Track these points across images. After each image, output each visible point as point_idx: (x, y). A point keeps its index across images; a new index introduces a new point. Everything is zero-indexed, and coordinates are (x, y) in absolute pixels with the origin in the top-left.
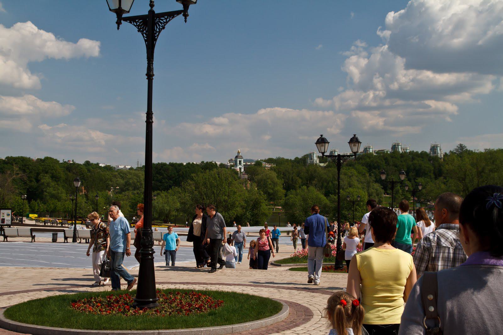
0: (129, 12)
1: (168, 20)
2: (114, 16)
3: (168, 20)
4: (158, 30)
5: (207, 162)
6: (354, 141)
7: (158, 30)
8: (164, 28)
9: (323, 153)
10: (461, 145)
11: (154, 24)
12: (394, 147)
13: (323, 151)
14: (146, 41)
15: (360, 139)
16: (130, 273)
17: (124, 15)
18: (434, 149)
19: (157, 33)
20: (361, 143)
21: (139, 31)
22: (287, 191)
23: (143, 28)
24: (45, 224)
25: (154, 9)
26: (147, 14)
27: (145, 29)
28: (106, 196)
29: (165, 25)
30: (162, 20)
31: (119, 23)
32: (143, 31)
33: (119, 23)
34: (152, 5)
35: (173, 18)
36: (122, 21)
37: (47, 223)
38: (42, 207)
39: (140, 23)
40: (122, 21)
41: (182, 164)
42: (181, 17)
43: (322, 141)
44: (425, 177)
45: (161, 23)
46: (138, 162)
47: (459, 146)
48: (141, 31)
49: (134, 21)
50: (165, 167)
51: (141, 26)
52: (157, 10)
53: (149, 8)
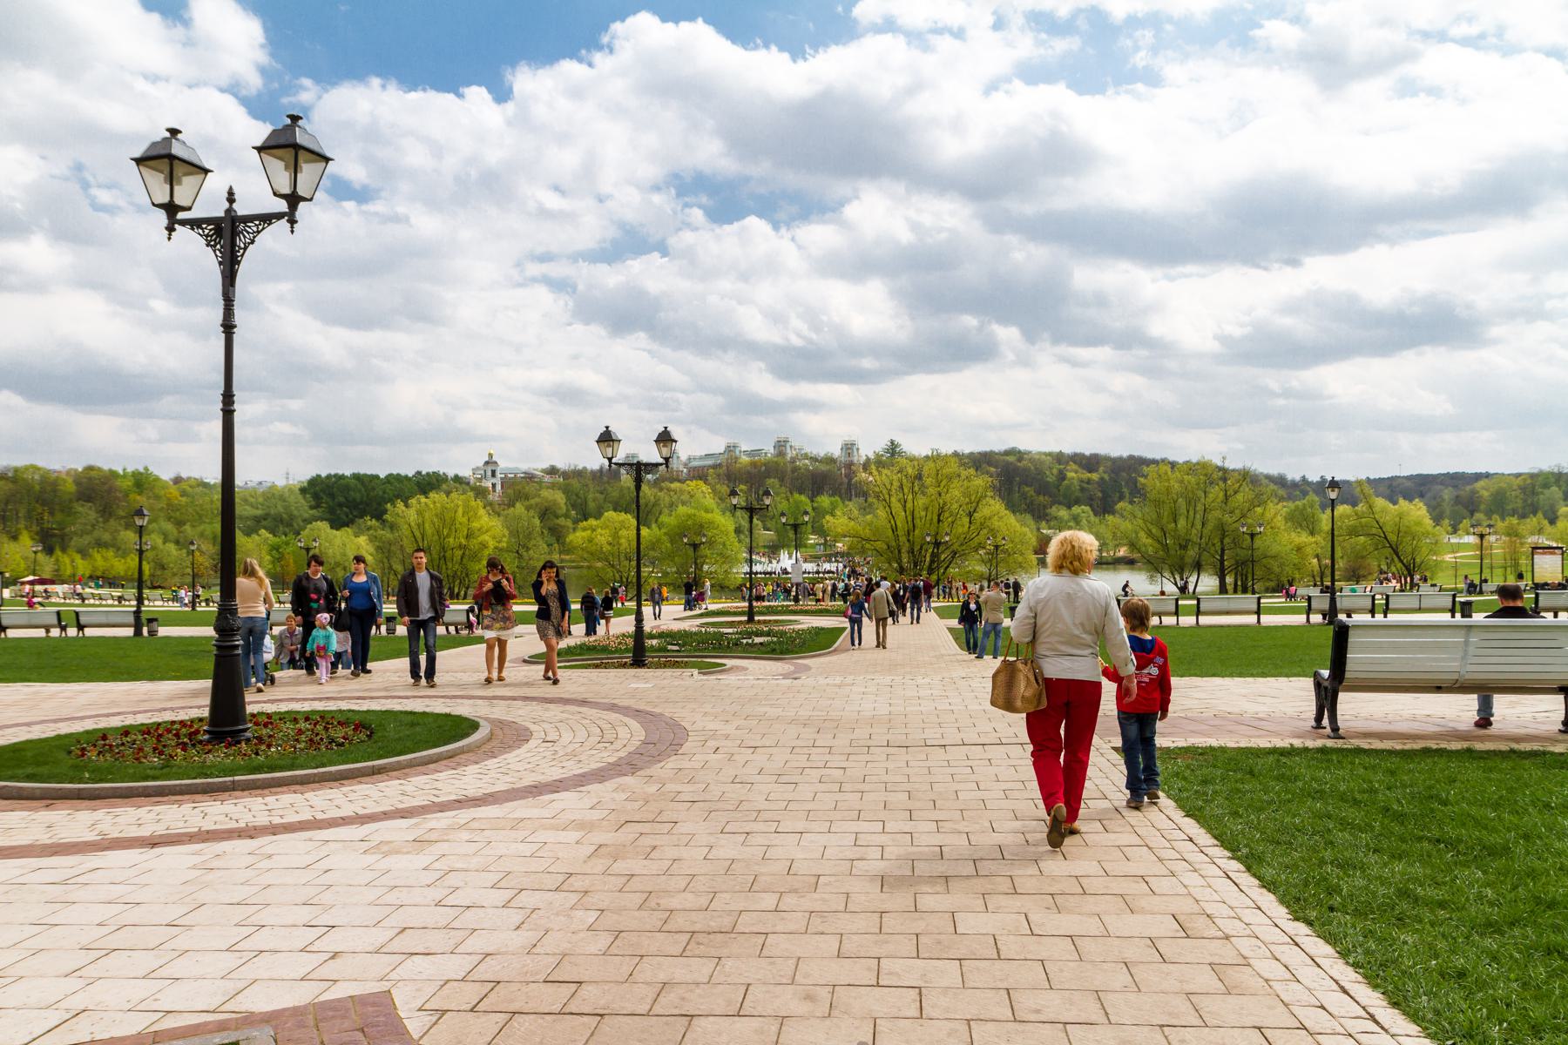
0: (189, 209)
1: (261, 227)
2: (161, 217)
3: (261, 227)
4: (242, 245)
5: (428, 474)
6: (665, 438)
7: (242, 245)
8: (253, 242)
9: (610, 460)
10: (892, 442)
11: (234, 233)
12: (781, 445)
13: (610, 456)
14: (220, 263)
15: (675, 436)
16: (635, 743)
17: (181, 215)
18: (849, 448)
19: (242, 251)
20: (676, 441)
21: (207, 246)
22: (42, 529)
23: (215, 240)
24: (120, 602)
25: (235, 206)
26: (222, 214)
27: (219, 242)
28: (1363, 557)
29: (254, 237)
30: (249, 227)
31: (170, 229)
32: (215, 246)
33: (170, 229)
34: (231, 198)
35: (269, 225)
36: (176, 226)
37: (88, 599)
38: (83, 567)
39: (211, 230)
40: (176, 226)
41: (377, 477)
42: (284, 222)
43: (606, 438)
44: (484, 508)
45: (248, 233)
46: (288, 474)
47: (889, 444)
48: (211, 246)
49: (199, 227)
50: (342, 481)
51: (211, 236)
52: (241, 209)
53: (227, 205)
